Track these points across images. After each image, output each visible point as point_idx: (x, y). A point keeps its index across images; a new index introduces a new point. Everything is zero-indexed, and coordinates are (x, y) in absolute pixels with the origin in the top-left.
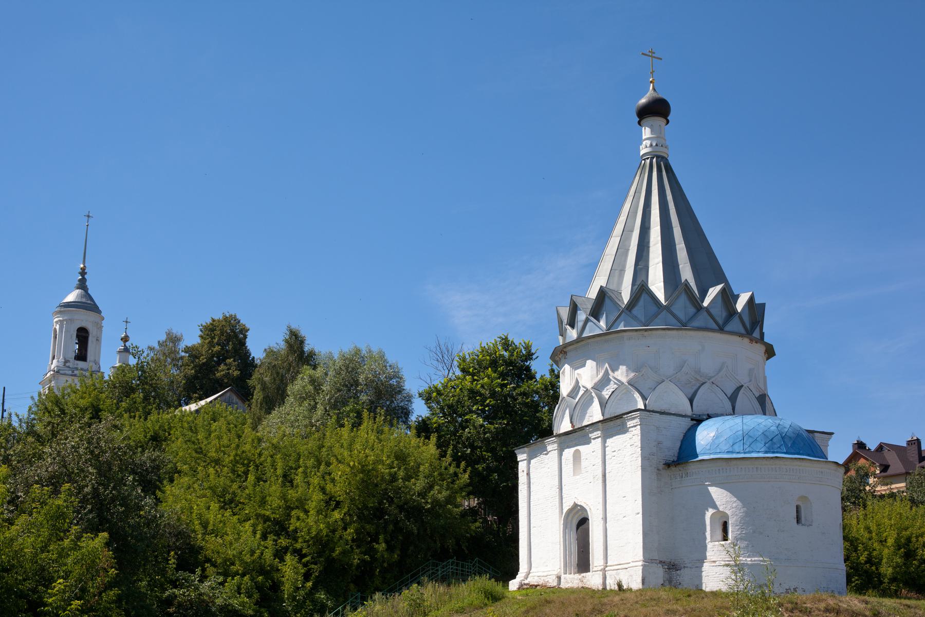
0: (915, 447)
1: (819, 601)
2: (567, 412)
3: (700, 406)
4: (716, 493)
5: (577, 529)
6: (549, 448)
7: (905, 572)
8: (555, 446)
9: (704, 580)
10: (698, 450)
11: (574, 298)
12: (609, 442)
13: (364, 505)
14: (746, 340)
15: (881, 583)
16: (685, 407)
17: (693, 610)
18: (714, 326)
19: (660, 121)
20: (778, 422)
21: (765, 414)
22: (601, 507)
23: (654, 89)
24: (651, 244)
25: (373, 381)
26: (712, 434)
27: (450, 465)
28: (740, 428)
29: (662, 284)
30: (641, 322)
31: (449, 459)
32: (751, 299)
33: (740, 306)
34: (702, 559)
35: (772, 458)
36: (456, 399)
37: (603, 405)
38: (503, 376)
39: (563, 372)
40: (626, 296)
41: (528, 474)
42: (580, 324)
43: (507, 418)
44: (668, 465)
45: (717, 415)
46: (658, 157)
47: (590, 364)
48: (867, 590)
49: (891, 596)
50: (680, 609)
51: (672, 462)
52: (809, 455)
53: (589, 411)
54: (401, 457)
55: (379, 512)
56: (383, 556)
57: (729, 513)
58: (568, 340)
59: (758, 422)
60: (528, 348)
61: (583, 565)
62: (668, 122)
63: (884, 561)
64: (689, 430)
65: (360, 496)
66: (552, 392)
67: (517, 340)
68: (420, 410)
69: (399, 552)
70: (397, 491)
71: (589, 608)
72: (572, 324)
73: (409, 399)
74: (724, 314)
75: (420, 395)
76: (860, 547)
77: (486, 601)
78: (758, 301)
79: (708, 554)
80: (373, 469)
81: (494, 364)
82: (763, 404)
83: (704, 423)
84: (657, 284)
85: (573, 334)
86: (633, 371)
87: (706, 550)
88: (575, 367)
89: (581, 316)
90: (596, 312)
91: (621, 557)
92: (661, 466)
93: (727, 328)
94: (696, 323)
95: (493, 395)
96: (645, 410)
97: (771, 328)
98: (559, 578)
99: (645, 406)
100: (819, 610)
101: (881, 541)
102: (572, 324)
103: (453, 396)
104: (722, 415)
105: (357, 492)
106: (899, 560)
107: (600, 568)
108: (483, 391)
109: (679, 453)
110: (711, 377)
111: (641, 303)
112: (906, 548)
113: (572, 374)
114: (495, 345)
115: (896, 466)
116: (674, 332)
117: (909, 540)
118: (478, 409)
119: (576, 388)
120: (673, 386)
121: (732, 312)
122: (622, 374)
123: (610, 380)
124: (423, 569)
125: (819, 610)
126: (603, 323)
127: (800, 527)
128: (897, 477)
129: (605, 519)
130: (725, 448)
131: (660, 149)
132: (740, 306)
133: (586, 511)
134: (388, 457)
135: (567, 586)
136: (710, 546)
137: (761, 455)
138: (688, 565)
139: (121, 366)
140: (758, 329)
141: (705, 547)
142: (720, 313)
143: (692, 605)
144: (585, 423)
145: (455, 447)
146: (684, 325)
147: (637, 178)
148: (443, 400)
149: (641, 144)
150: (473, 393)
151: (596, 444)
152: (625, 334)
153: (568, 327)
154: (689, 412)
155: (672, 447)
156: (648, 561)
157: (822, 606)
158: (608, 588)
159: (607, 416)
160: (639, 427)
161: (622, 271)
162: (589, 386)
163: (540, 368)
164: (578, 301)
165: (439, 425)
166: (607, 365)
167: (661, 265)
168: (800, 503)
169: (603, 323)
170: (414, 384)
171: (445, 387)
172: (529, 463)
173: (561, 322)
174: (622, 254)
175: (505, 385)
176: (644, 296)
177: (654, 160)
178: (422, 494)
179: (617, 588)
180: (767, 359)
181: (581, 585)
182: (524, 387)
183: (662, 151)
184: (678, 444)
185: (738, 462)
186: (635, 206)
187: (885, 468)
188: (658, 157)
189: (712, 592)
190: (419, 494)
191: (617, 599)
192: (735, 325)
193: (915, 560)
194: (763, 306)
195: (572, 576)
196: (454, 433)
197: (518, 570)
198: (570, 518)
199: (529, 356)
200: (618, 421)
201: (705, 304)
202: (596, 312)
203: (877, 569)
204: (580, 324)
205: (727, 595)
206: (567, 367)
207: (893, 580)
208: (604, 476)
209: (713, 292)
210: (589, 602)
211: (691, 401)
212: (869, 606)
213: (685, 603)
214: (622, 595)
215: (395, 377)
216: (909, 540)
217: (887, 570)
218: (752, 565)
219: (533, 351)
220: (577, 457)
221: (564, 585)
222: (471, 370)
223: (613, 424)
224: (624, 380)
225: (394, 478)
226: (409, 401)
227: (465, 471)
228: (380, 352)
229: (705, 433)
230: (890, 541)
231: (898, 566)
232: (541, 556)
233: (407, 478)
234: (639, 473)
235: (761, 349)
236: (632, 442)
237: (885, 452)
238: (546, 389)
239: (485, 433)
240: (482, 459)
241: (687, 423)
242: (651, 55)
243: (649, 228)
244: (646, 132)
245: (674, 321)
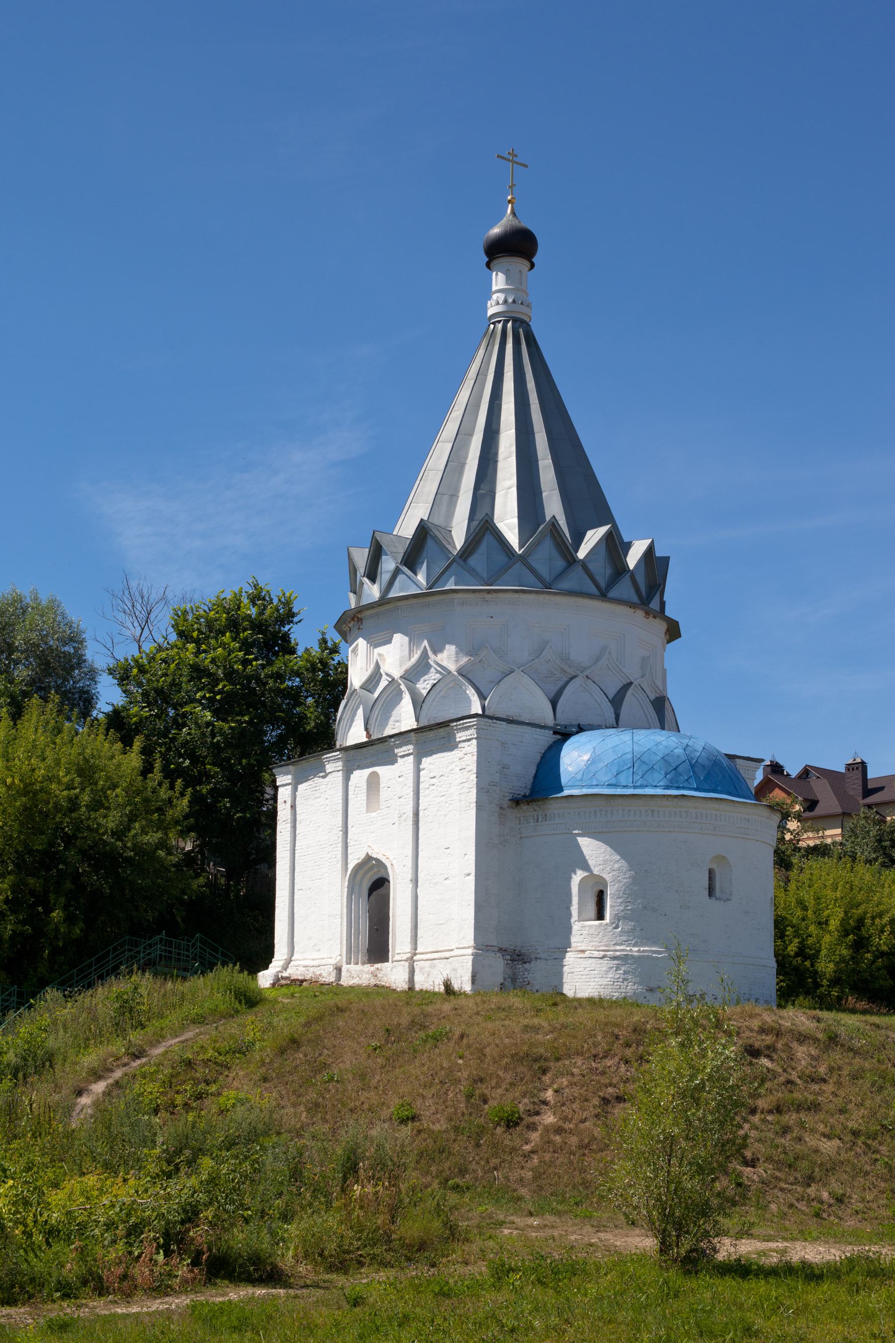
0: (858, 774)
1: (751, 1016)
2: (360, 712)
3: (567, 713)
4: (589, 846)
5: (370, 894)
6: (329, 767)
7: (853, 970)
8: (339, 765)
9: (566, 978)
10: (564, 780)
11: (378, 535)
12: (426, 762)
13: (26, 846)
14: (640, 614)
15: (817, 985)
16: (545, 713)
17: (564, 1026)
18: (594, 590)
19: (520, 264)
20: (685, 741)
21: (663, 728)
22: (409, 862)
23: (513, 213)
24: (501, 457)
25: (38, 646)
26: (586, 757)
27: (160, 784)
28: (629, 749)
29: (515, 521)
30: (482, 578)
31: (157, 775)
32: (650, 550)
33: (633, 559)
34: (564, 946)
35: (676, 796)
36: (169, 679)
37: (418, 704)
38: (246, 646)
39: (355, 651)
40: (459, 538)
41: (293, 807)
42: (385, 577)
43: (249, 713)
44: (517, 802)
45: (592, 727)
46: (515, 320)
47: (399, 639)
48: (797, 996)
49: (829, 1009)
50: (545, 1024)
51: (523, 797)
52: (730, 794)
53: (395, 713)
54: (86, 771)
55: (49, 858)
56: (57, 929)
57: (607, 877)
58: (365, 601)
59: (653, 741)
60: (287, 603)
61: (378, 949)
62: (532, 266)
63: (824, 952)
64: (550, 748)
65: (20, 832)
66: (321, 675)
67: (275, 590)
68: (109, 696)
69: (81, 925)
70: (78, 825)
71: (405, 1020)
72: (372, 575)
73: (92, 674)
74: (609, 571)
75: (111, 672)
76: (789, 931)
77: (237, 1005)
78: (659, 553)
79: (573, 939)
80: (41, 790)
81: (234, 625)
82: (661, 712)
83: (573, 739)
84: (507, 519)
85: (373, 592)
86: (467, 655)
87: (570, 932)
88: (375, 643)
89: (388, 565)
90: (411, 560)
91: (440, 941)
92: (506, 803)
93: (611, 594)
94: (566, 584)
95: (230, 675)
96: (483, 715)
97: (676, 597)
98: (339, 970)
99: (483, 708)
100: (752, 1030)
101: (820, 923)
102: (372, 575)
103: (166, 675)
104: (599, 727)
105: (16, 826)
106: (845, 952)
107: (405, 957)
108: (212, 668)
109: (533, 783)
110: (585, 669)
111: (483, 549)
112: (856, 933)
113: (369, 655)
114: (237, 599)
115: (829, 803)
116: (532, 597)
117: (861, 922)
118: (204, 697)
119: (376, 676)
120: (526, 680)
121: (620, 569)
122: (449, 658)
123: (430, 667)
124: (115, 949)
125: (752, 1030)
126: (421, 578)
127: (713, 901)
128: (828, 820)
129: (415, 881)
130: (605, 778)
131: (518, 308)
132: (633, 559)
133: (385, 867)
134: (68, 773)
135: (351, 982)
136: (576, 927)
137: (659, 791)
138: (542, 955)
140: (657, 599)
141: (569, 929)
142: (602, 570)
143: (562, 1019)
144: (388, 731)
145: (164, 756)
146: (547, 586)
147: (481, 352)
148: (149, 681)
149: (490, 298)
150: (198, 672)
151: (405, 765)
152: (456, 596)
153: (366, 580)
154: (550, 721)
155: (522, 775)
156: (482, 948)
157: (755, 1024)
158: (418, 987)
159: (421, 725)
160: (474, 742)
161: (454, 497)
162: (397, 674)
163: (305, 638)
164: (384, 540)
165: (141, 720)
166: (425, 643)
167: (514, 490)
168: (714, 866)
169: (421, 578)
170: (97, 656)
171: (152, 659)
172: (295, 790)
173: (353, 570)
174: (456, 472)
175: (250, 662)
176: (488, 539)
177: (510, 325)
178: (119, 834)
179: (442, 988)
180: (668, 642)
181: (373, 982)
182: (278, 664)
183: (521, 312)
184: (533, 771)
185: (620, 801)
186: (475, 397)
187: (811, 805)
188: (515, 320)
189: (590, 1000)
190: (113, 834)
191: (447, 1007)
192: (624, 589)
193: (868, 952)
194: (666, 560)
195: (359, 967)
196: (165, 734)
197: (271, 955)
198: (358, 878)
199: (289, 616)
200: (442, 732)
201: (581, 554)
202: (411, 560)
203: (812, 965)
204: (385, 576)
205: (613, 1004)
206: (361, 643)
207: (836, 981)
208: (416, 814)
209: (593, 537)
210: (405, 1010)
211: (554, 703)
212: (822, 1025)
213: (551, 1016)
214: (454, 1002)
215: (71, 640)
216: (861, 922)
217: (826, 967)
218: (639, 957)
219: (295, 610)
220: (373, 783)
221: (346, 981)
222: (195, 634)
223: (433, 735)
224: (452, 667)
225: (74, 804)
226: (93, 679)
227: (182, 794)
228: (53, 601)
229: (575, 754)
230: (834, 924)
231: (843, 960)
232: (310, 936)
233: (97, 804)
234: (473, 812)
235: (660, 627)
236: (463, 764)
237: (813, 779)
238: (313, 669)
239: (213, 735)
240: (205, 776)
241: (546, 738)
242: (512, 158)
243: (497, 432)
244: (498, 281)
245: (533, 579)
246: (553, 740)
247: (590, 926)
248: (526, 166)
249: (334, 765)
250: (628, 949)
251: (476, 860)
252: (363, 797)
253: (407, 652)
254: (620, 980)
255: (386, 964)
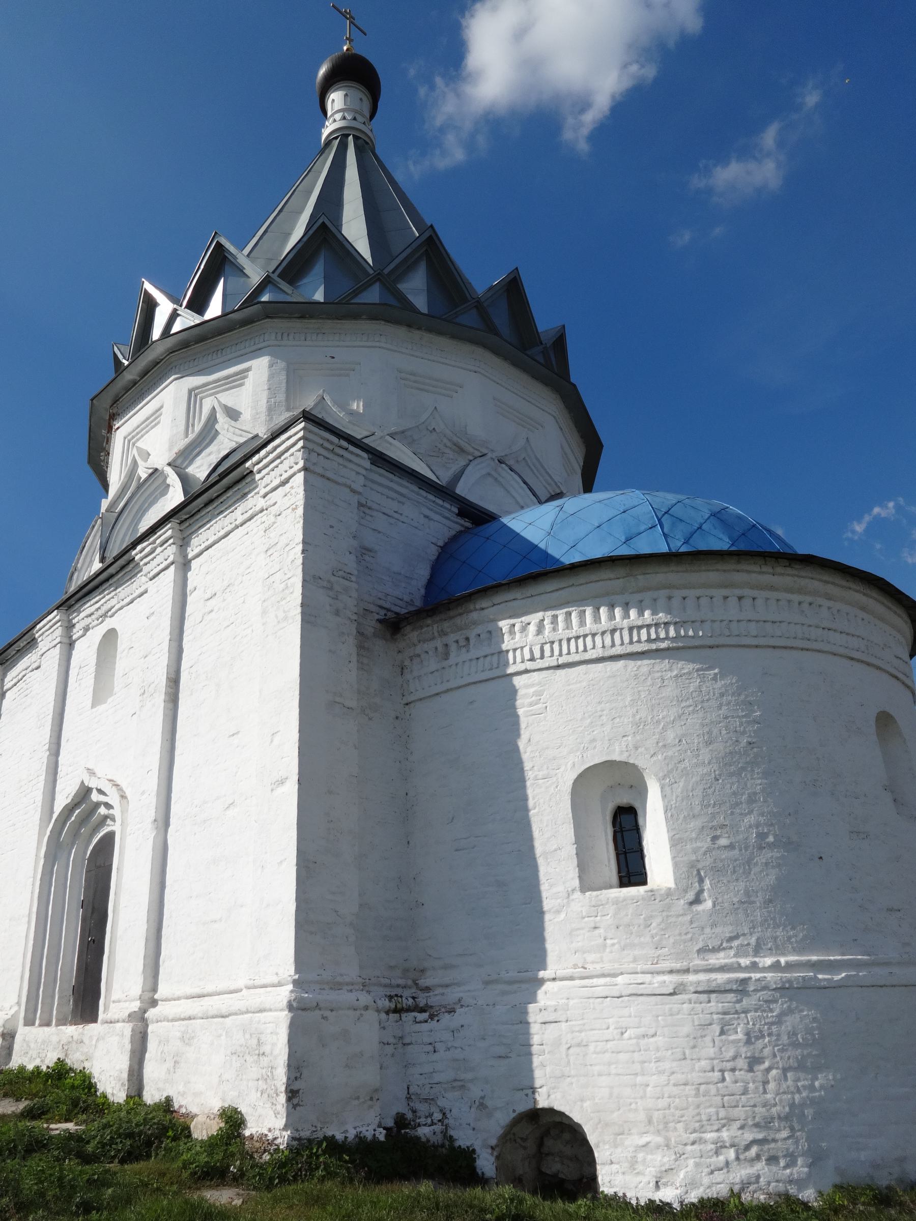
22: (152, 783)
44: (394, 625)
84: (354, 228)
92: (370, 626)
129: (164, 821)
139: (766, 774)
184: (423, 573)
208: (174, 681)
246: (458, 528)
247: (616, 902)
248: (365, 34)
249: (50, 638)
250: (745, 961)
251: (301, 740)
252: (89, 681)
253: (182, 427)
254: (741, 1063)
255: (92, 1026)
